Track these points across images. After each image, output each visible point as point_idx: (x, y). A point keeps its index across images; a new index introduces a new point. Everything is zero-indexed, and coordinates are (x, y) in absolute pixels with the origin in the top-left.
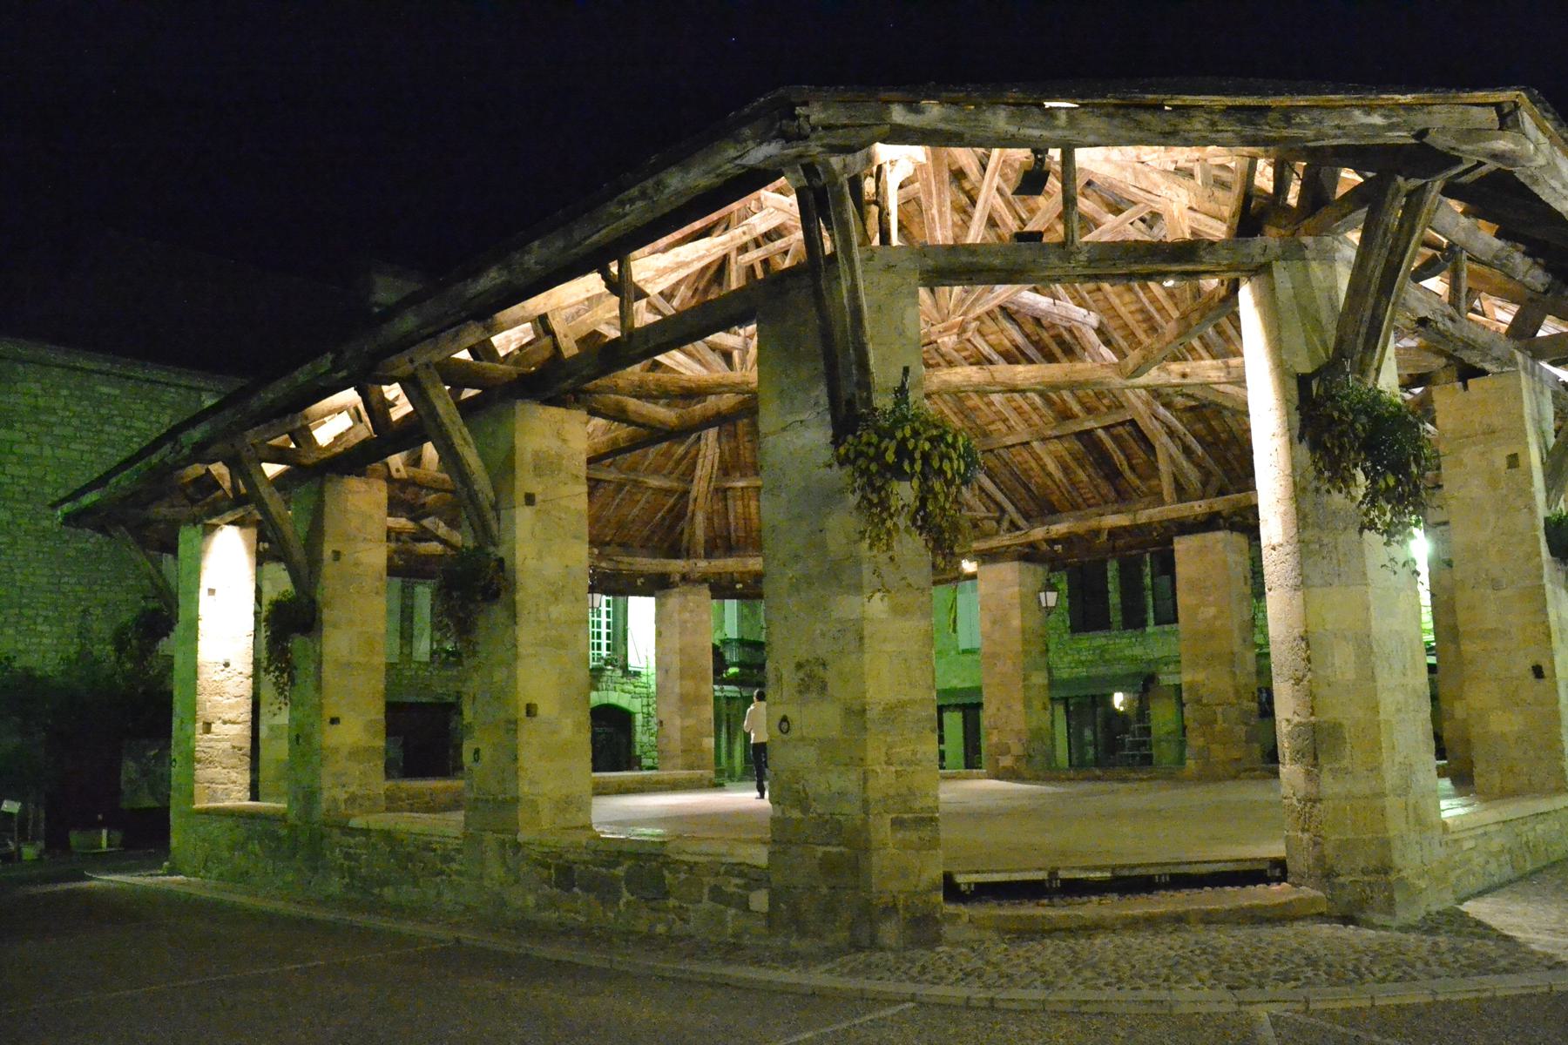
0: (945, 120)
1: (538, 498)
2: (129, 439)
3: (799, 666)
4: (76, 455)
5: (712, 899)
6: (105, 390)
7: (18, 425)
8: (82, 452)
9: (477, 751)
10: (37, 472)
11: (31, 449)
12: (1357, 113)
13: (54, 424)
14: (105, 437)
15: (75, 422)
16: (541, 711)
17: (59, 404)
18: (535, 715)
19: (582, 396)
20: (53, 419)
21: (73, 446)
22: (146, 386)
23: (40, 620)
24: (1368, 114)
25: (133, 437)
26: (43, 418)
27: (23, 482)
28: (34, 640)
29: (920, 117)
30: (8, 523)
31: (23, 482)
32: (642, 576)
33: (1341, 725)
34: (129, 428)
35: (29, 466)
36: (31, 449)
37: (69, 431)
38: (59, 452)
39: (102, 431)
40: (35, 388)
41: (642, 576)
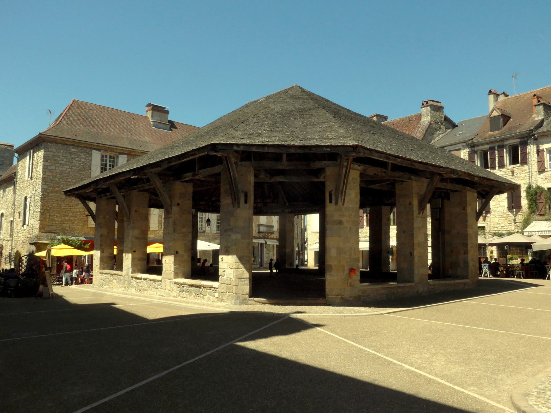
0: (244, 149)
1: (180, 204)
2: (80, 164)
3: (225, 248)
4: (65, 169)
5: (209, 294)
6: (73, 150)
7: (49, 161)
8: (67, 168)
9: (165, 261)
10: (54, 174)
11: (53, 168)
12: (324, 148)
13: (59, 160)
14: (73, 164)
15: (65, 160)
16: (179, 252)
17: (60, 154)
18: (178, 253)
19: (217, 146)
20: (59, 159)
21: (64, 167)
22: (85, 149)
23: (55, 217)
24: (327, 148)
25: (81, 164)
26: (56, 158)
27: (50, 177)
28: (53, 222)
29: (239, 148)
30: (47, 189)
31: (50, 177)
32: (374, 116)
33: (332, 265)
34: (80, 161)
35: (52, 172)
36: (53, 168)
37: (63, 162)
38: (60, 169)
39: (72, 162)
40: (54, 150)
41: (374, 116)
